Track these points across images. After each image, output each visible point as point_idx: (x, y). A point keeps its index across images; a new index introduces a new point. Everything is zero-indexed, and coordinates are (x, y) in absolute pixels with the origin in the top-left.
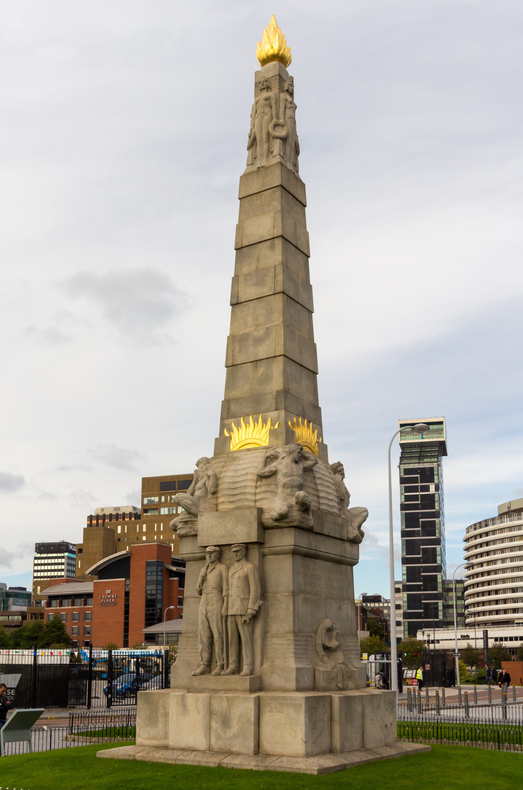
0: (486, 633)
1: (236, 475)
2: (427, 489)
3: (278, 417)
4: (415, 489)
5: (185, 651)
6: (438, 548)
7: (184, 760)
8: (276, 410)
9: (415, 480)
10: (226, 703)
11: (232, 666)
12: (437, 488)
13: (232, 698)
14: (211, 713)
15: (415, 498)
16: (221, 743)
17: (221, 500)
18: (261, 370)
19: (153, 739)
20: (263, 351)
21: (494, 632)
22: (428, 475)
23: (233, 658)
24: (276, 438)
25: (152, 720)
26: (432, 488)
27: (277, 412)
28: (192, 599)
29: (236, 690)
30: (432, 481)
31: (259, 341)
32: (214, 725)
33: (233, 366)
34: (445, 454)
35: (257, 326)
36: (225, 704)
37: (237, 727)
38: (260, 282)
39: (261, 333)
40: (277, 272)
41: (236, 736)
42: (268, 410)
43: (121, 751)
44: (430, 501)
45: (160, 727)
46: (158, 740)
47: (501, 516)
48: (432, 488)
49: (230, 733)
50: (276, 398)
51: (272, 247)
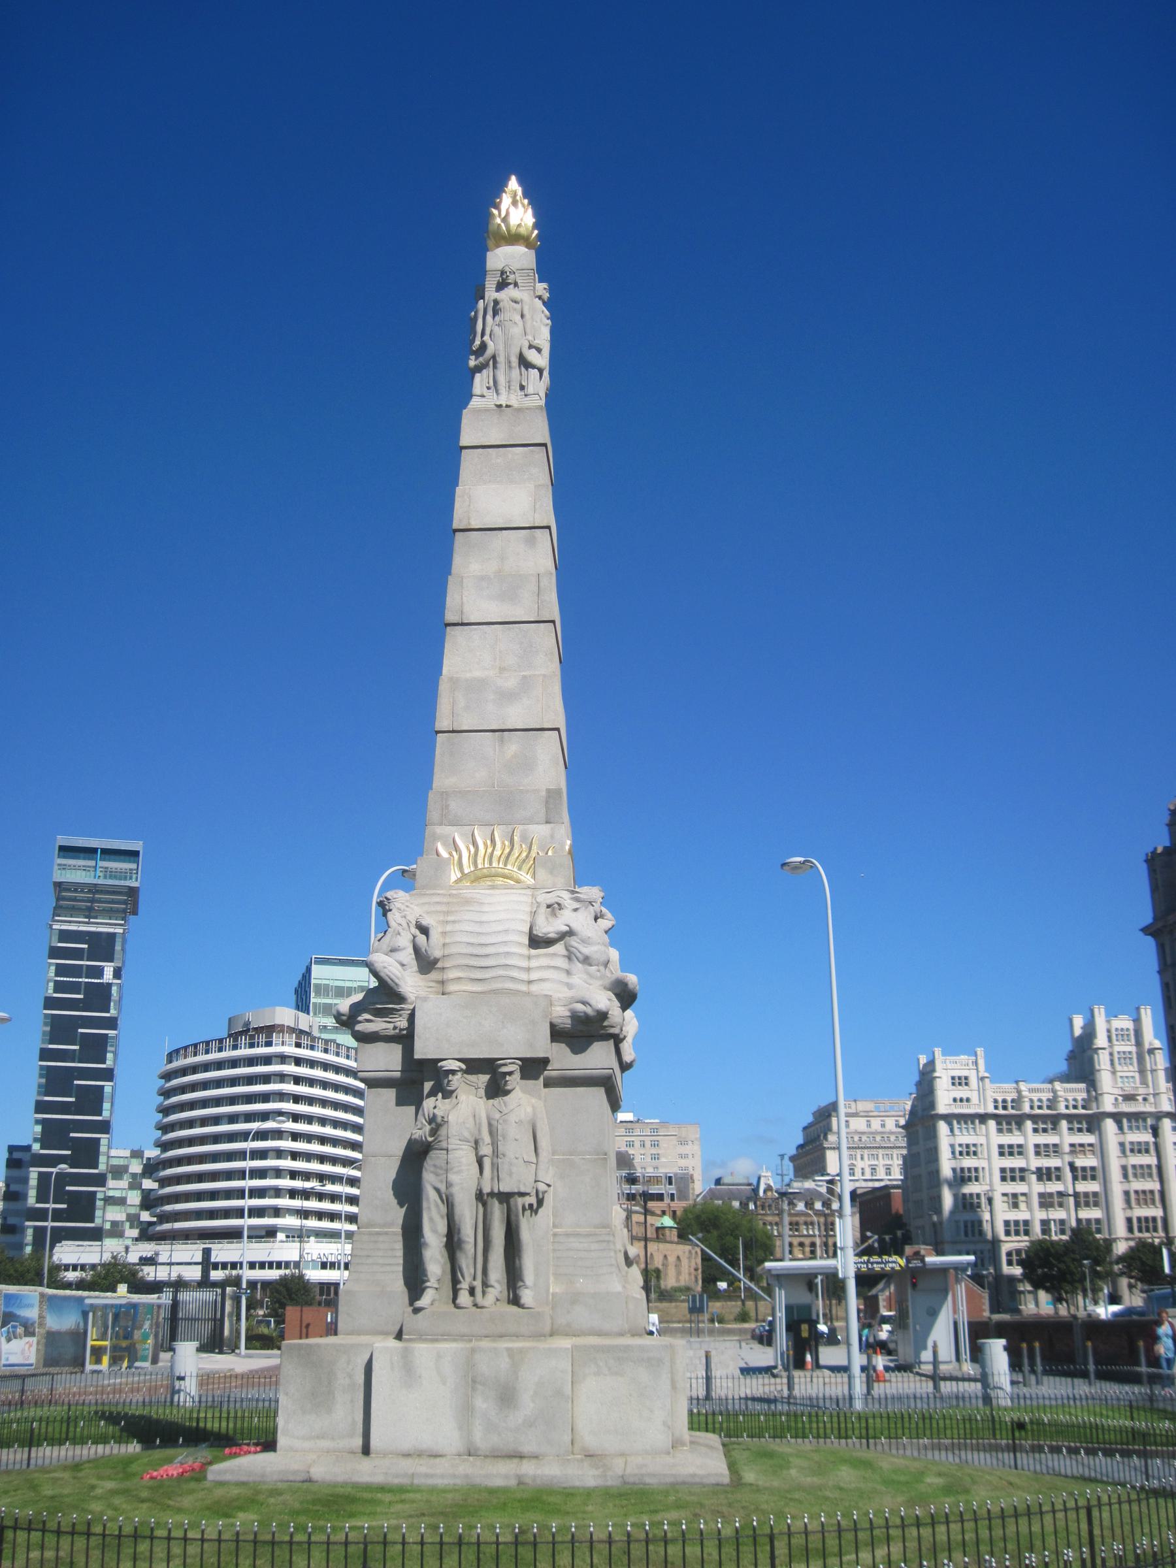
0: (207, 1253)
1: (480, 930)
2: (99, 972)
3: (552, 836)
5: (370, 1261)
6: (108, 1086)
7: (432, 1476)
8: (547, 822)
10: (507, 1360)
12: (117, 973)
13: (521, 1351)
14: (472, 1381)
15: (74, 987)
19: (321, 1436)
20: (516, 716)
21: (223, 1252)
24: (551, 873)
27: (548, 826)
28: (383, 1159)
29: (517, 1336)
30: (110, 959)
31: (508, 697)
32: (482, 1404)
33: (453, 731)
34: (135, 912)
35: (502, 670)
36: (504, 1363)
37: (532, 1405)
38: (510, 594)
39: (510, 682)
40: (542, 585)
41: (530, 1424)
42: (531, 821)
43: (250, 1465)
44: (99, 996)
46: (333, 1439)
47: (235, 1036)
50: (547, 802)
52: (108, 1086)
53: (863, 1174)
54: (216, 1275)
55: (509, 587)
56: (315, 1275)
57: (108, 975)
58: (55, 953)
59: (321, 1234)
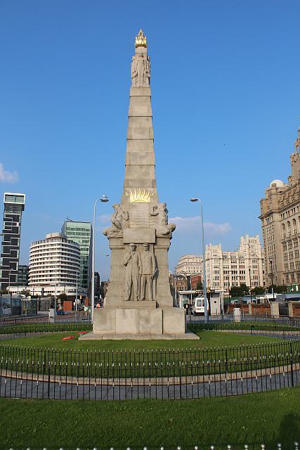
4: (10, 224)
6: (18, 251)
9: (10, 220)
11: (142, 297)
12: (20, 224)
14: (139, 317)
16: (144, 330)
17: (131, 223)
18: (144, 170)
19: (104, 330)
20: (144, 162)
22: (16, 218)
23: (142, 294)
25: (103, 321)
26: (18, 224)
31: (142, 157)
36: (147, 313)
38: (143, 133)
39: (143, 154)
41: (153, 327)
42: (149, 187)
44: (16, 230)
45: (108, 324)
48: (18, 224)
49: (149, 326)
51: (147, 120)
52: (18, 251)
53: (86, 242)
54: (45, 294)
55: (142, 131)
56: (68, 294)
57: (18, 225)
58: (5, 219)
59: (68, 285)
